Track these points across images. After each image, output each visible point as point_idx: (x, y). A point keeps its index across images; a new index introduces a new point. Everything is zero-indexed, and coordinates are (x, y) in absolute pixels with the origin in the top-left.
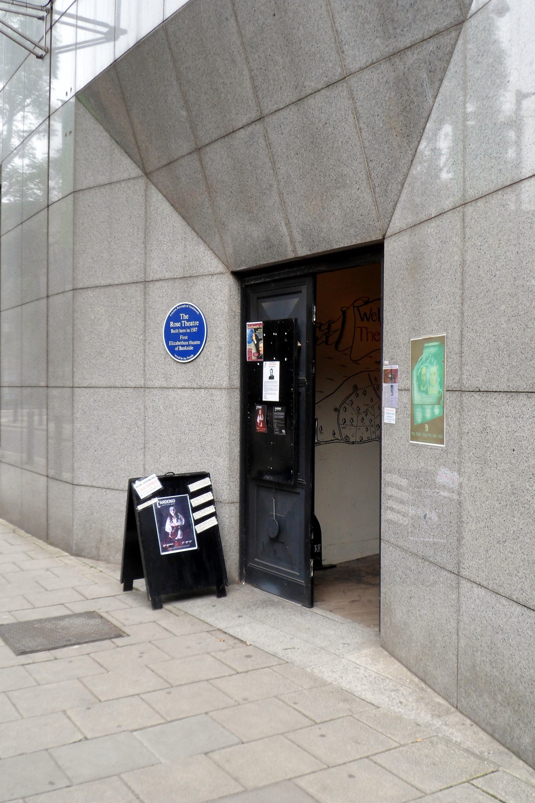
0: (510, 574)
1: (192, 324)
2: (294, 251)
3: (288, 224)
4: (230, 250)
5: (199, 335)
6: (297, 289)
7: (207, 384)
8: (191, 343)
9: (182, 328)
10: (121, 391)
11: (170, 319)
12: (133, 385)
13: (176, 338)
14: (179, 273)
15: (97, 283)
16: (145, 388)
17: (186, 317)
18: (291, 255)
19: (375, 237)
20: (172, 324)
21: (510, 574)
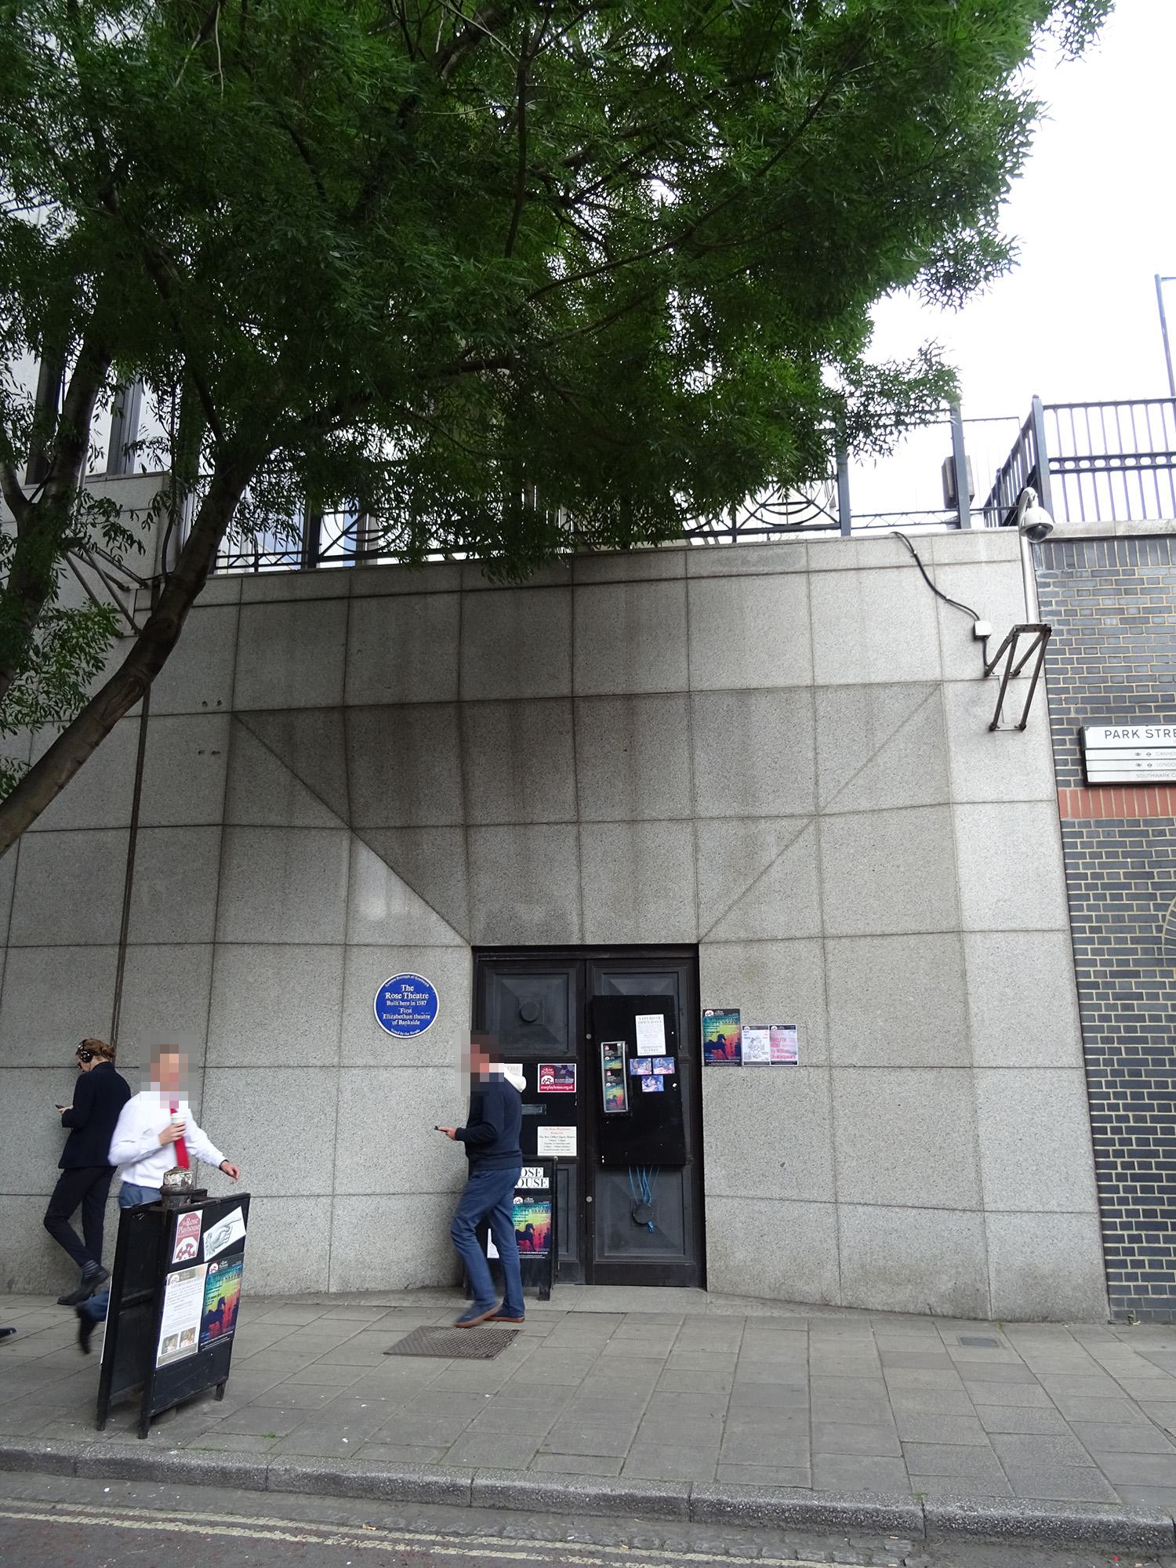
0: (903, 1189)
1: (418, 996)
2: (583, 938)
3: (581, 915)
4: (480, 926)
5: (431, 1007)
6: (565, 970)
7: (436, 1061)
8: (417, 1016)
9: (403, 1000)
10: (297, 1072)
11: (384, 990)
12: (319, 1063)
13: (395, 1010)
14: (399, 940)
15: (261, 939)
16: (341, 1067)
17: (412, 989)
18: (575, 941)
19: (691, 940)
20: (388, 995)
21: (903, 1189)
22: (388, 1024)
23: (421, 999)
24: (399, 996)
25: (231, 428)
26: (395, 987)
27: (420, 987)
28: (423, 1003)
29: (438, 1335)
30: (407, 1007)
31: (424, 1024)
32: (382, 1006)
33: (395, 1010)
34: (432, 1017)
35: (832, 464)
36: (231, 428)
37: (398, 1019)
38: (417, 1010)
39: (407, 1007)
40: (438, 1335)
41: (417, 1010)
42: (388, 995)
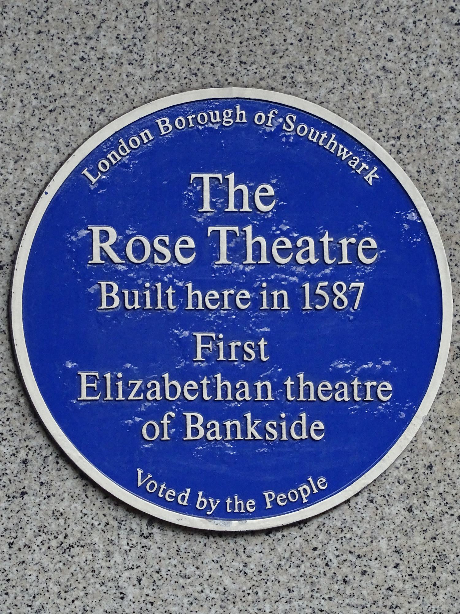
1: (308, 250)
8: (303, 386)
9: (202, 271)
11: (74, 206)
13: (154, 342)
17: (263, 197)
20: (102, 242)
22: (108, 437)
23: (332, 265)
24: (180, 251)
25: (211, 317)
26: (149, 182)
27: (323, 184)
28: (343, 296)
29: (209, 214)
30: (234, 326)
31: (356, 441)
32: (63, 317)
33: (154, 342)
34: (411, 391)
35: (346, 310)
36: (211, 317)
37: (168, 402)
38: (303, 342)
39: (234, 326)
40: (209, 214)
41: (303, 342)
42: (102, 242)
